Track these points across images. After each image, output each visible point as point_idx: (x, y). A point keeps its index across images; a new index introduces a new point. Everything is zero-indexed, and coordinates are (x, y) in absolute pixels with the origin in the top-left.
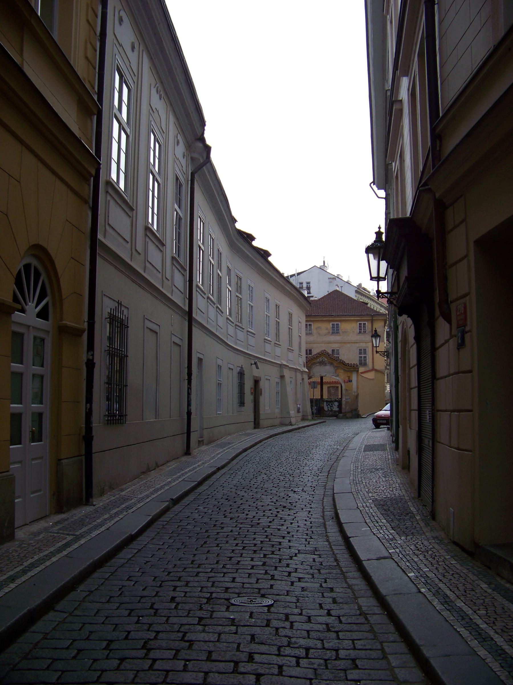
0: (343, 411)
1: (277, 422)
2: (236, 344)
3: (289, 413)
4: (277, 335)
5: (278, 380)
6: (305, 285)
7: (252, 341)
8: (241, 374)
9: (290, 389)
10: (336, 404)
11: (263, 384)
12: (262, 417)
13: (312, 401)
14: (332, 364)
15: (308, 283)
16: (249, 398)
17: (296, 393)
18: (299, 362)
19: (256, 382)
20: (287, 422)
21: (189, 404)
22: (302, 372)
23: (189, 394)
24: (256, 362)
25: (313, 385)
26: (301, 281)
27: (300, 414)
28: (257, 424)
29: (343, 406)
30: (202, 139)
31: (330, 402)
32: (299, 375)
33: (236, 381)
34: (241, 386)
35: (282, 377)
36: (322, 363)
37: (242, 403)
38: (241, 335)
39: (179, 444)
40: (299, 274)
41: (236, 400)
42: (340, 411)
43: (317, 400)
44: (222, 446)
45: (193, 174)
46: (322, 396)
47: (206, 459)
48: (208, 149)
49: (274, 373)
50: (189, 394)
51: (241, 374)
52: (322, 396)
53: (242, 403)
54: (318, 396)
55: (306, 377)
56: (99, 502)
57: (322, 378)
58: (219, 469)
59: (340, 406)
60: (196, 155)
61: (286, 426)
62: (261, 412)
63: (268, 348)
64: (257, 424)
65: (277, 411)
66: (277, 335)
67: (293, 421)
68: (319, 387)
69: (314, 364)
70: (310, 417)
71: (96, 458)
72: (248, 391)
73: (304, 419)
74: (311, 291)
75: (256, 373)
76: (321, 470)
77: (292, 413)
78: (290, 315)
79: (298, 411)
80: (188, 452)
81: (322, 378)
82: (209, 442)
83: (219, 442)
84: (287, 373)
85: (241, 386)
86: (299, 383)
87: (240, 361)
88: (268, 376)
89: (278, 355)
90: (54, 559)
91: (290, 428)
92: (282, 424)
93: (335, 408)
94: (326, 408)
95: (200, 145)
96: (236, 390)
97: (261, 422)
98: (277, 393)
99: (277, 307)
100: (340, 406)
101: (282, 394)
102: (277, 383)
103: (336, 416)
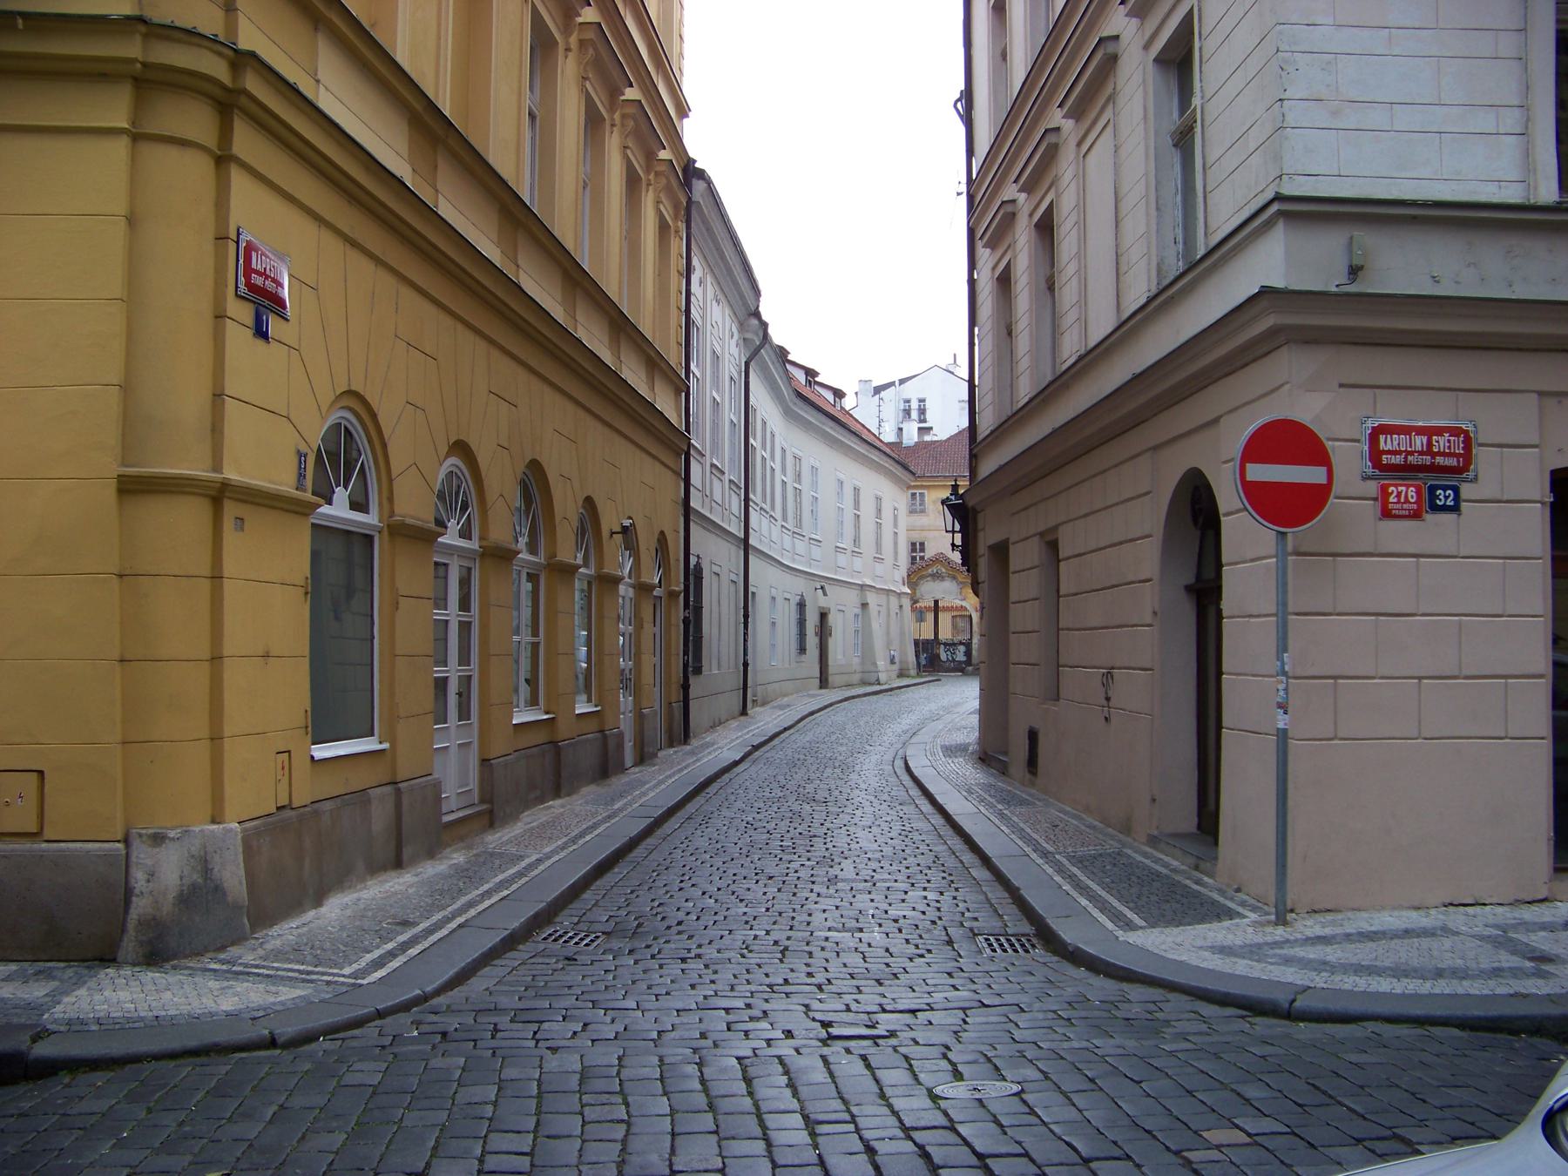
0: (974, 661)
1: (856, 678)
2: (794, 560)
3: (875, 664)
4: (856, 541)
5: (858, 611)
6: (914, 405)
7: (816, 552)
8: (801, 606)
9: (877, 626)
10: (962, 648)
11: (834, 619)
12: (831, 670)
13: (916, 643)
14: (954, 578)
15: (922, 401)
16: (812, 641)
17: (888, 633)
18: (893, 575)
19: (823, 616)
20: (873, 680)
21: (745, 654)
22: (900, 595)
23: (745, 640)
24: (824, 584)
25: (920, 615)
26: (907, 397)
27: (896, 667)
28: (824, 682)
29: (974, 653)
30: (757, 314)
31: (950, 645)
32: (894, 600)
33: (794, 616)
34: (802, 623)
35: (864, 605)
36: (937, 577)
37: (802, 650)
38: (801, 546)
39: (735, 701)
40: (902, 381)
41: (794, 646)
42: (969, 662)
43: (927, 642)
44: (781, 707)
45: (747, 365)
46: (936, 634)
47: (765, 720)
48: (764, 325)
49: (851, 599)
50: (745, 640)
51: (801, 606)
52: (936, 634)
53: (802, 650)
54: (928, 634)
55: (907, 603)
56: (695, 743)
57: (936, 602)
58: (786, 729)
59: (968, 653)
60: (749, 336)
61: (871, 686)
62: (830, 662)
63: (842, 560)
64: (824, 682)
65: (856, 661)
66: (856, 541)
67: (883, 677)
68: (930, 616)
69: (922, 577)
70: (913, 672)
71: (694, 706)
72: (814, 630)
73: (901, 675)
74: (928, 416)
75: (823, 602)
76: (905, 732)
77: (882, 663)
78: (879, 499)
79: (892, 662)
80: (744, 712)
81: (936, 602)
82: (763, 704)
83: (774, 704)
84: (872, 599)
85: (802, 623)
86: (893, 614)
87: (798, 586)
88: (842, 606)
89: (860, 570)
90: (588, 838)
91: (877, 688)
92: (864, 683)
93: (961, 657)
94: (943, 657)
95: (755, 322)
96: (794, 630)
97: (830, 679)
98: (857, 631)
99: (856, 490)
100: (968, 653)
101: (864, 634)
102: (856, 616)
103: (962, 671)
